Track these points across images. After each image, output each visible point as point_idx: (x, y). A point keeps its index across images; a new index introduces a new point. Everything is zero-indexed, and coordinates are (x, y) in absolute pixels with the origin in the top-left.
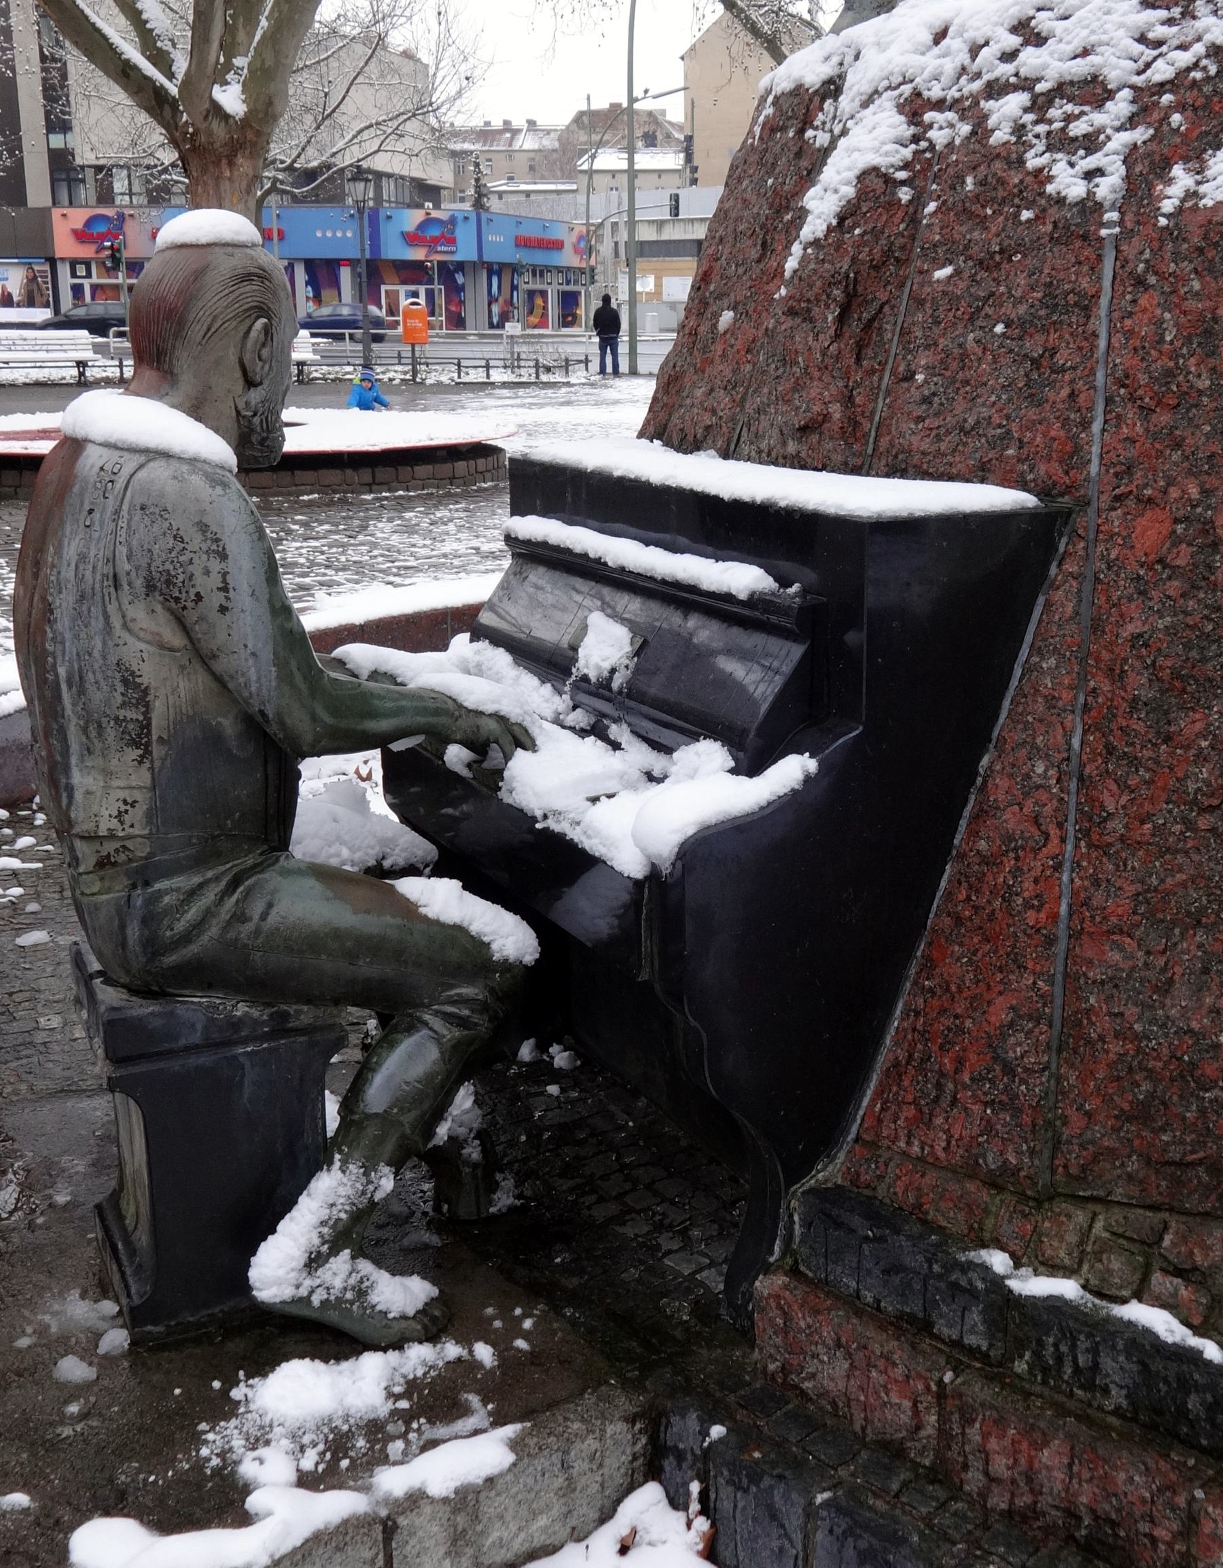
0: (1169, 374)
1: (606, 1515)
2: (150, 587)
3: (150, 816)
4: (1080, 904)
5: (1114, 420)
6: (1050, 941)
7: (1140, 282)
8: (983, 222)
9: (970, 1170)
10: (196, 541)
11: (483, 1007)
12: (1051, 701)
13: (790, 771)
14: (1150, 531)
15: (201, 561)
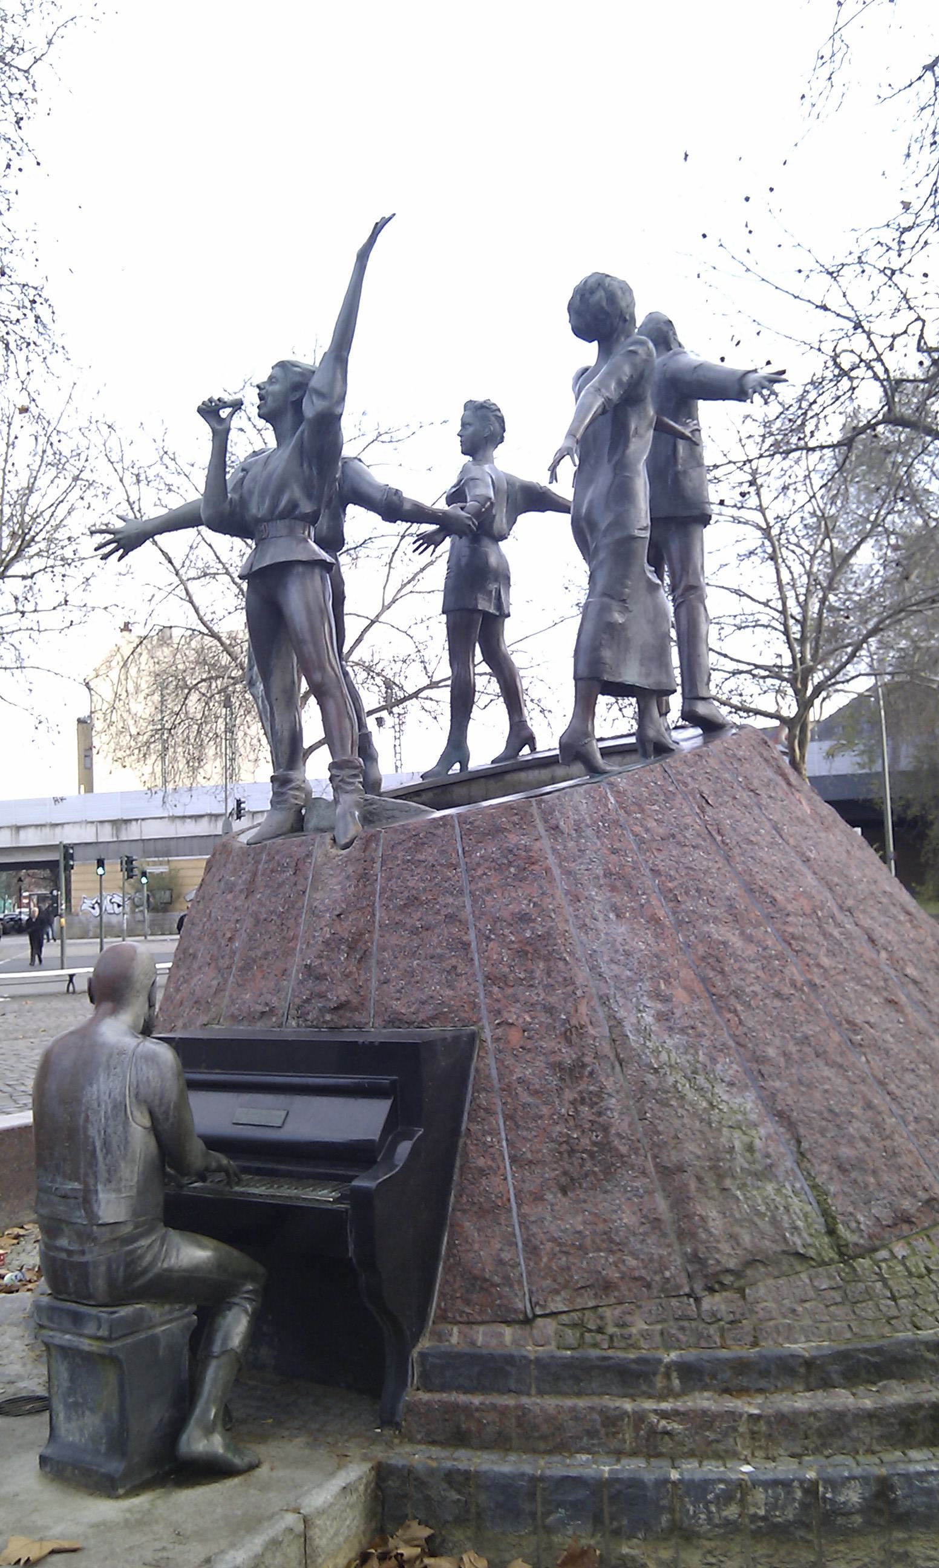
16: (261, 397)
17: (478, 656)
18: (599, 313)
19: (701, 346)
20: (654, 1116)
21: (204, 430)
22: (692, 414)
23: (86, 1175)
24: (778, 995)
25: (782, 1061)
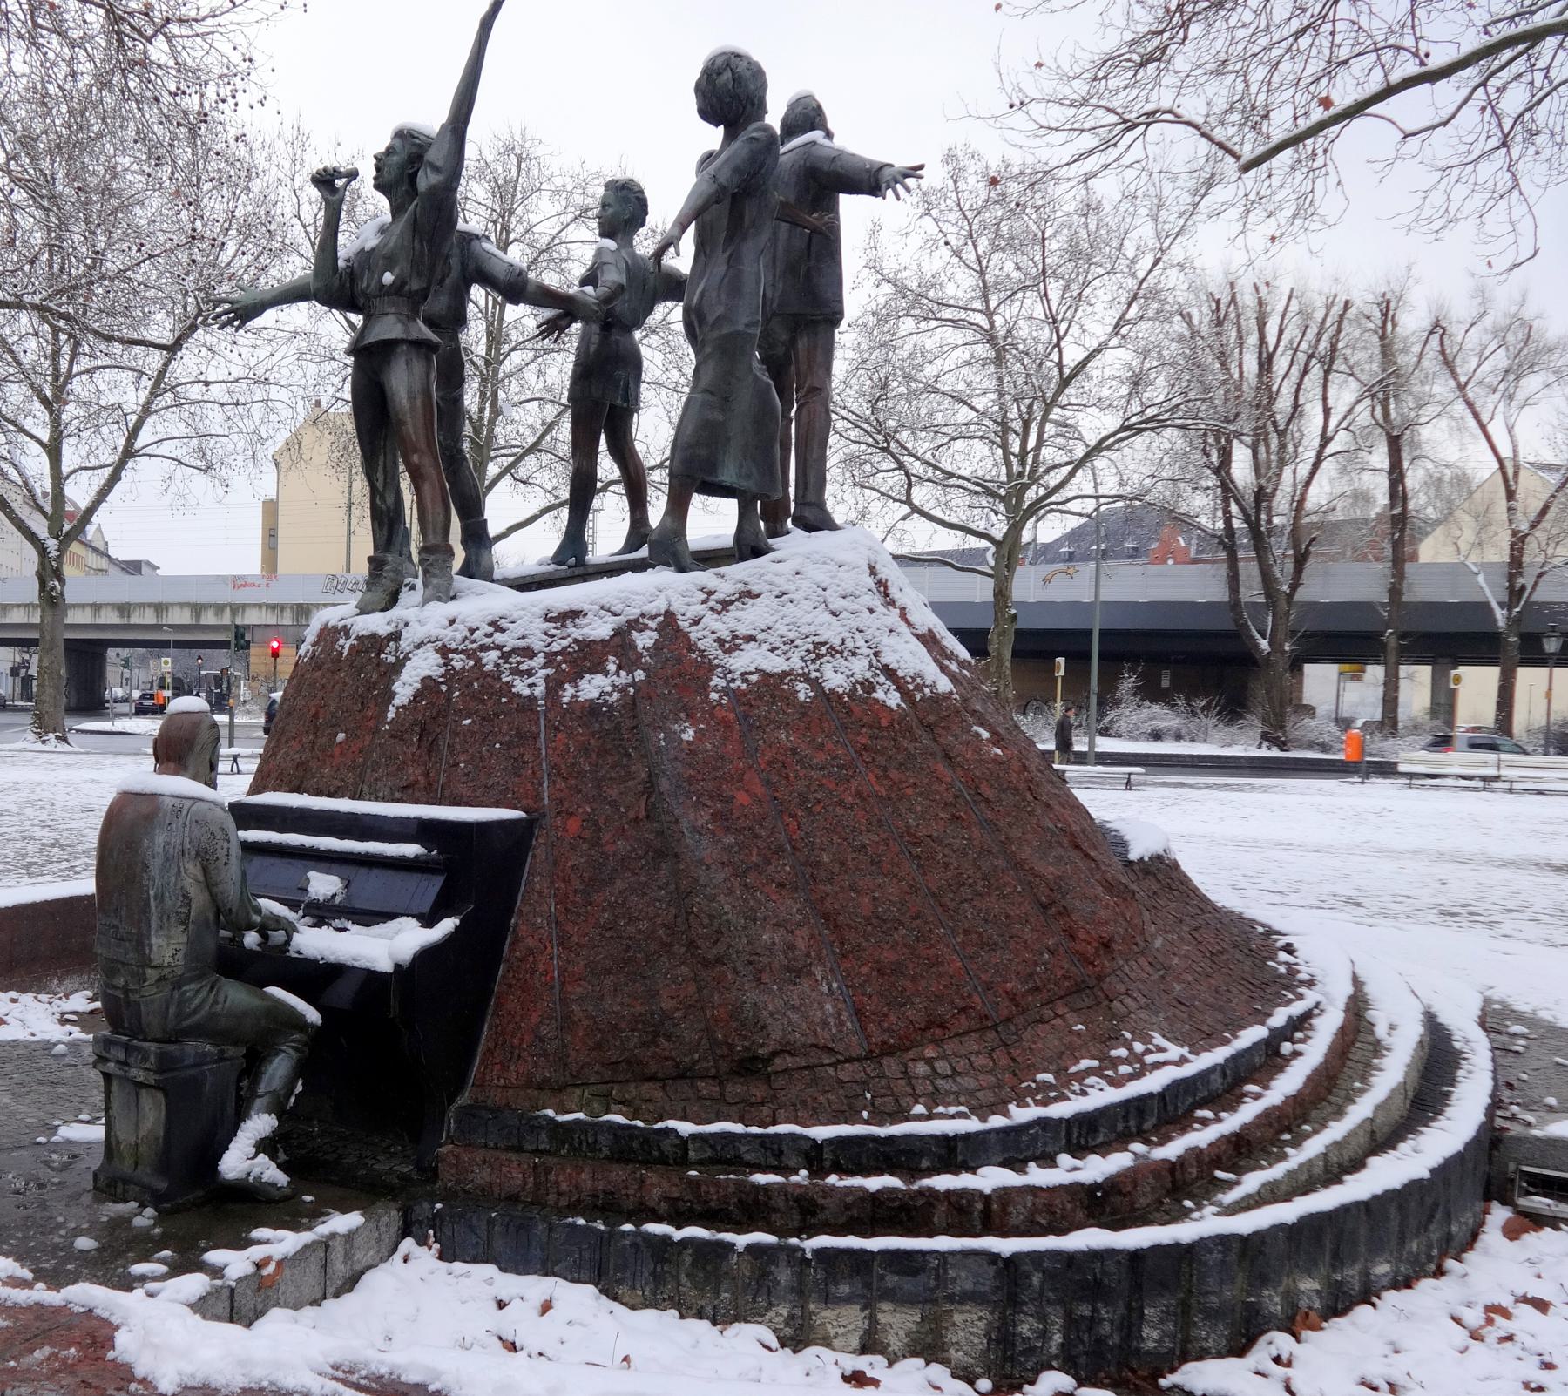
0: (573, 764)
1: (394, 1250)
2: (198, 854)
3: (185, 956)
4: (562, 972)
5: (552, 783)
6: (552, 988)
7: (557, 729)
8: (483, 702)
9: (529, 1084)
10: (219, 835)
11: (306, 1044)
12: (540, 894)
13: (447, 925)
14: (574, 825)
15: (221, 843)
16: (378, 169)
17: (402, 468)
18: (728, 92)
19: (853, 135)
20: (701, 910)
21: (311, 201)
22: (833, 208)
23: (140, 921)
24: (841, 803)
25: (836, 868)
